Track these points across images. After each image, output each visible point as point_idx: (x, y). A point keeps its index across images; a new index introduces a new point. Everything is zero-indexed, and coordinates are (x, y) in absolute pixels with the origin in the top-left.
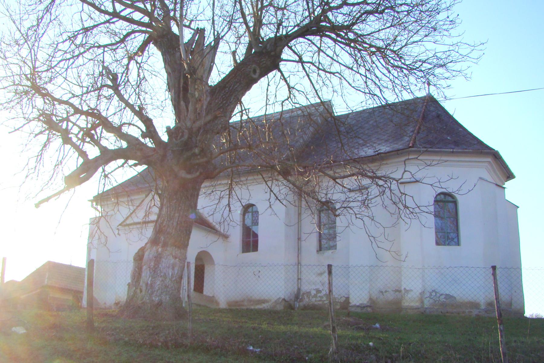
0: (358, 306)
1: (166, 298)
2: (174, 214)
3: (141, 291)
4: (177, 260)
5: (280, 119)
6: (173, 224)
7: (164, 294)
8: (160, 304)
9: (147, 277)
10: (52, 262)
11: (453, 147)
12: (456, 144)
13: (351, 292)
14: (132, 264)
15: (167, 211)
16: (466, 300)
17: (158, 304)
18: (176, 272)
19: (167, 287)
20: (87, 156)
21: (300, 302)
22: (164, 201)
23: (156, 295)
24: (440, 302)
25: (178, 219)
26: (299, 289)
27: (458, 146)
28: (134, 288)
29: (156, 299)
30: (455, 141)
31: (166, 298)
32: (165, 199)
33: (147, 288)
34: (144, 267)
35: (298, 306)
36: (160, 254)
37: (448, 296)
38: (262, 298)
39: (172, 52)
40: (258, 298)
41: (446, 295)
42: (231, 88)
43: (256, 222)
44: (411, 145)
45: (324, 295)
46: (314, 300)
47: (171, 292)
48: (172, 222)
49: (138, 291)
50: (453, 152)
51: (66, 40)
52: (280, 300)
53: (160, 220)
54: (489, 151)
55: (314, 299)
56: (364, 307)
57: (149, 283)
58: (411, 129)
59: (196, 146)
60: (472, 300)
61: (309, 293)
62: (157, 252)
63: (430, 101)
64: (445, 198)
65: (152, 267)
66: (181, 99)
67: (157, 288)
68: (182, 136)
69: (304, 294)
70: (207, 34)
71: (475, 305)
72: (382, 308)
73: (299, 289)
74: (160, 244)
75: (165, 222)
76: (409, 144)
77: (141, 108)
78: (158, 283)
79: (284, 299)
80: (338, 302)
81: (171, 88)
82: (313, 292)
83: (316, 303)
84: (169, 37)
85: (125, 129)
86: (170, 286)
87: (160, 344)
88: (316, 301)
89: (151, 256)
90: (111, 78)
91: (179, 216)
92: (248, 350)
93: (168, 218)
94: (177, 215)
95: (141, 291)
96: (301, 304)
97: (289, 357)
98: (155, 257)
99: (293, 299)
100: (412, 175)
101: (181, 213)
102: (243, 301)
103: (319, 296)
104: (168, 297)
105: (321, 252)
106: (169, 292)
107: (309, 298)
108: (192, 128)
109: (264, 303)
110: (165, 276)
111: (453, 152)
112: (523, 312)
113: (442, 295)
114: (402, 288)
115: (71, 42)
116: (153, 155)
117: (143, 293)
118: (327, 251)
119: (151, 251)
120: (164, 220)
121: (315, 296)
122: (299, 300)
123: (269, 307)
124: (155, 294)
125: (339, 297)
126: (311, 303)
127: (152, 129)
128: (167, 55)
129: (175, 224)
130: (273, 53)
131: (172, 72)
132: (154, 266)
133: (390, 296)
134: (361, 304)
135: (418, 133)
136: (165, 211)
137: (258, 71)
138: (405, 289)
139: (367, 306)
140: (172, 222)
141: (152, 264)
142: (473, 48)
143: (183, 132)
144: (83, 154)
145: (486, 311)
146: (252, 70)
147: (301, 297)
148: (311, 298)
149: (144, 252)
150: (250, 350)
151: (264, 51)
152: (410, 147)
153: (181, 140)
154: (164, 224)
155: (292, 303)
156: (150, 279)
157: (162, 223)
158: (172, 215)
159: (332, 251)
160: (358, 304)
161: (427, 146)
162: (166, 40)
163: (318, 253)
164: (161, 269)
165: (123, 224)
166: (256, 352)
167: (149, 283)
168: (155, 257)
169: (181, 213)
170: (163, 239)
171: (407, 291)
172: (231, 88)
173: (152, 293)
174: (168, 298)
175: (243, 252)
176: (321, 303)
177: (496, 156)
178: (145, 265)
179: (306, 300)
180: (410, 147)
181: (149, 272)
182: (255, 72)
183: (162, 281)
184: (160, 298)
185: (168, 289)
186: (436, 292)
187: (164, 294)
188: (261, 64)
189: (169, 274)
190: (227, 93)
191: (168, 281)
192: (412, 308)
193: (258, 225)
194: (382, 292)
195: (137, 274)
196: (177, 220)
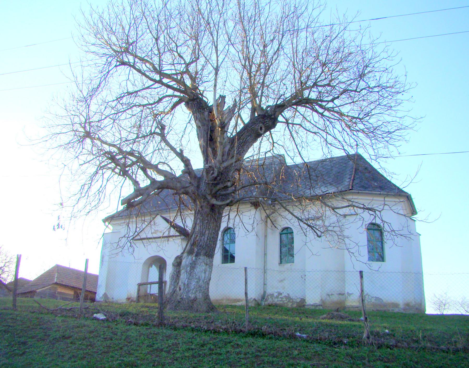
0: (312, 305)
1: (200, 296)
2: (205, 231)
3: (180, 289)
4: (208, 266)
5: (263, 165)
6: (204, 239)
7: (198, 292)
8: (195, 300)
9: (184, 278)
10: (61, 266)
11: (380, 190)
12: (381, 188)
13: (306, 294)
14: (171, 270)
15: (200, 229)
16: (389, 301)
17: (194, 299)
18: (207, 276)
19: (200, 286)
20: (139, 184)
21: (265, 301)
22: (197, 221)
23: (192, 293)
24: (371, 303)
25: (208, 235)
26: (265, 292)
27: (383, 190)
28: (173, 287)
29: (192, 296)
30: (380, 187)
31: (200, 296)
32: (198, 220)
33: (184, 287)
34: (182, 271)
35: (263, 304)
36: (194, 262)
37: (377, 298)
38: (238, 298)
39: (202, 112)
40: (235, 298)
41: (376, 297)
42: (244, 140)
43: (233, 241)
44: (350, 188)
45: (284, 297)
46: (276, 300)
47: (203, 290)
48: (203, 237)
49: (178, 289)
50: (380, 194)
51: (115, 100)
52: (252, 300)
53: (194, 236)
54: (405, 194)
55: (277, 299)
56: (317, 306)
57: (186, 283)
58: (348, 177)
59: (229, 181)
60: (393, 301)
61: (272, 295)
62: (192, 260)
63: (358, 158)
64: (287, 231)
65: (188, 271)
66: (209, 146)
67: (193, 287)
68: (213, 173)
69: (268, 295)
70: (226, 100)
71: (396, 305)
72: (329, 307)
73: (265, 292)
74: (194, 254)
75: (198, 237)
76: (349, 188)
77: (182, 151)
78: (194, 284)
79: (255, 299)
80: (295, 302)
81: (200, 137)
82: (276, 294)
83: (278, 302)
84: (198, 100)
85: (160, 167)
86: (202, 287)
87: (221, 330)
88: (278, 301)
89: (187, 263)
90: (160, 128)
91: (209, 233)
92: (296, 335)
93: (200, 234)
94: (207, 232)
95: (180, 289)
96: (266, 303)
97: (332, 340)
98: (190, 264)
99: (260, 298)
100: (390, 208)
101: (211, 231)
102: (222, 300)
103: (281, 298)
104: (201, 294)
105: (282, 264)
106: (201, 290)
107: (272, 299)
108: (220, 167)
109: (239, 301)
110: (199, 278)
111: (380, 194)
112: (424, 311)
113: (373, 297)
114: (346, 292)
115: (118, 101)
116: (189, 186)
117: (182, 291)
118: (287, 264)
119: (187, 259)
120: (197, 236)
121: (277, 297)
122: (264, 300)
123: (243, 304)
124: (191, 292)
125: (296, 298)
126: (274, 302)
127: (190, 167)
128: (198, 114)
129: (206, 239)
130: (273, 117)
131: (202, 126)
132: (190, 271)
133: (335, 298)
134: (315, 304)
135: (354, 180)
136: (198, 229)
137: (263, 129)
138: (348, 293)
139: (319, 305)
140: (203, 237)
141: (189, 268)
142: (415, 120)
143: (213, 170)
144: (136, 183)
145: (404, 309)
146: (259, 128)
147: (266, 298)
148: (274, 298)
149: (181, 260)
150: (298, 336)
151: (266, 114)
152: (350, 190)
153: (212, 176)
154: (197, 239)
155: (260, 302)
156: (187, 280)
157: (196, 238)
158: (204, 232)
159: (290, 264)
160: (312, 304)
161: (361, 189)
162: (196, 102)
163: (279, 265)
164: (196, 273)
165: (134, 239)
166: (303, 337)
167: (186, 283)
168: (190, 264)
169: (211, 231)
170: (196, 250)
171: (349, 294)
172: (244, 140)
173: (189, 291)
174: (201, 296)
175: (222, 263)
176: (281, 302)
177: (408, 198)
178: (183, 269)
179: (270, 301)
180: (350, 190)
181: (186, 275)
182: (261, 129)
183: (197, 282)
184: (195, 295)
185: (201, 289)
186: (369, 295)
187: (198, 292)
188: (265, 123)
189: (202, 277)
190: (242, 143)
191: (201, 283)
192: (353, 307)
193: (235, 242)
194: (329, 295)
195: (175, 276)
196: (207, 236)
